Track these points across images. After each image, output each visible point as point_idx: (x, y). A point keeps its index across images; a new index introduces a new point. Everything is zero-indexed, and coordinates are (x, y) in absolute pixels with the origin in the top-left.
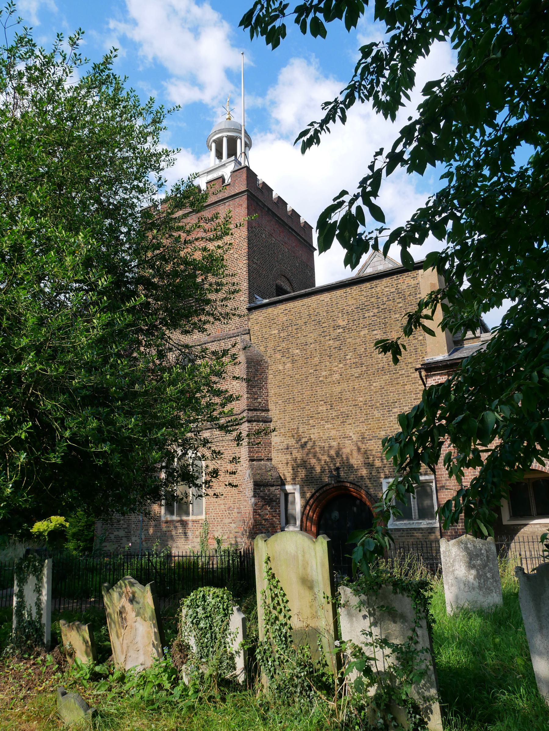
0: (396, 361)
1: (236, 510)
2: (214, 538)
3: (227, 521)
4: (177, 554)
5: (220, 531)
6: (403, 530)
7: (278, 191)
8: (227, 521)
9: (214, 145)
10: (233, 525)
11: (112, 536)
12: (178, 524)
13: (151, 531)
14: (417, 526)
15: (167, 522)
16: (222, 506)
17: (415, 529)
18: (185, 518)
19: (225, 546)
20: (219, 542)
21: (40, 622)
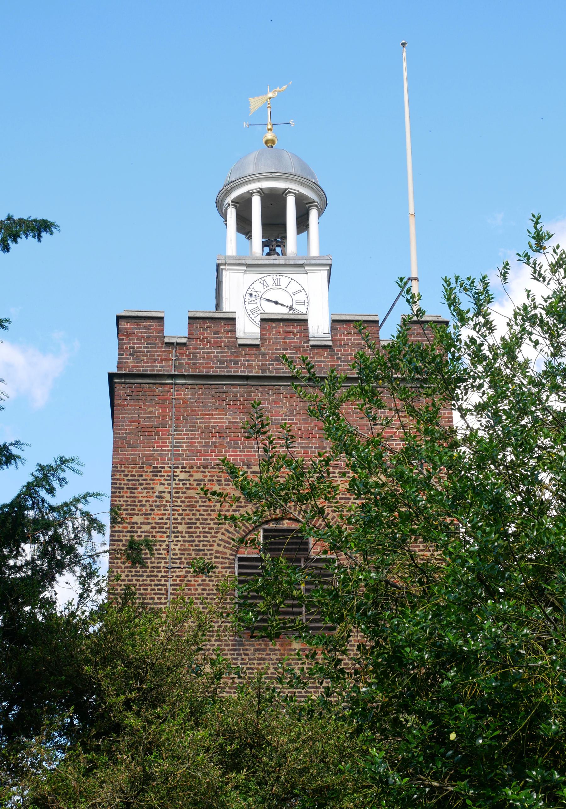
9: (232, 213)
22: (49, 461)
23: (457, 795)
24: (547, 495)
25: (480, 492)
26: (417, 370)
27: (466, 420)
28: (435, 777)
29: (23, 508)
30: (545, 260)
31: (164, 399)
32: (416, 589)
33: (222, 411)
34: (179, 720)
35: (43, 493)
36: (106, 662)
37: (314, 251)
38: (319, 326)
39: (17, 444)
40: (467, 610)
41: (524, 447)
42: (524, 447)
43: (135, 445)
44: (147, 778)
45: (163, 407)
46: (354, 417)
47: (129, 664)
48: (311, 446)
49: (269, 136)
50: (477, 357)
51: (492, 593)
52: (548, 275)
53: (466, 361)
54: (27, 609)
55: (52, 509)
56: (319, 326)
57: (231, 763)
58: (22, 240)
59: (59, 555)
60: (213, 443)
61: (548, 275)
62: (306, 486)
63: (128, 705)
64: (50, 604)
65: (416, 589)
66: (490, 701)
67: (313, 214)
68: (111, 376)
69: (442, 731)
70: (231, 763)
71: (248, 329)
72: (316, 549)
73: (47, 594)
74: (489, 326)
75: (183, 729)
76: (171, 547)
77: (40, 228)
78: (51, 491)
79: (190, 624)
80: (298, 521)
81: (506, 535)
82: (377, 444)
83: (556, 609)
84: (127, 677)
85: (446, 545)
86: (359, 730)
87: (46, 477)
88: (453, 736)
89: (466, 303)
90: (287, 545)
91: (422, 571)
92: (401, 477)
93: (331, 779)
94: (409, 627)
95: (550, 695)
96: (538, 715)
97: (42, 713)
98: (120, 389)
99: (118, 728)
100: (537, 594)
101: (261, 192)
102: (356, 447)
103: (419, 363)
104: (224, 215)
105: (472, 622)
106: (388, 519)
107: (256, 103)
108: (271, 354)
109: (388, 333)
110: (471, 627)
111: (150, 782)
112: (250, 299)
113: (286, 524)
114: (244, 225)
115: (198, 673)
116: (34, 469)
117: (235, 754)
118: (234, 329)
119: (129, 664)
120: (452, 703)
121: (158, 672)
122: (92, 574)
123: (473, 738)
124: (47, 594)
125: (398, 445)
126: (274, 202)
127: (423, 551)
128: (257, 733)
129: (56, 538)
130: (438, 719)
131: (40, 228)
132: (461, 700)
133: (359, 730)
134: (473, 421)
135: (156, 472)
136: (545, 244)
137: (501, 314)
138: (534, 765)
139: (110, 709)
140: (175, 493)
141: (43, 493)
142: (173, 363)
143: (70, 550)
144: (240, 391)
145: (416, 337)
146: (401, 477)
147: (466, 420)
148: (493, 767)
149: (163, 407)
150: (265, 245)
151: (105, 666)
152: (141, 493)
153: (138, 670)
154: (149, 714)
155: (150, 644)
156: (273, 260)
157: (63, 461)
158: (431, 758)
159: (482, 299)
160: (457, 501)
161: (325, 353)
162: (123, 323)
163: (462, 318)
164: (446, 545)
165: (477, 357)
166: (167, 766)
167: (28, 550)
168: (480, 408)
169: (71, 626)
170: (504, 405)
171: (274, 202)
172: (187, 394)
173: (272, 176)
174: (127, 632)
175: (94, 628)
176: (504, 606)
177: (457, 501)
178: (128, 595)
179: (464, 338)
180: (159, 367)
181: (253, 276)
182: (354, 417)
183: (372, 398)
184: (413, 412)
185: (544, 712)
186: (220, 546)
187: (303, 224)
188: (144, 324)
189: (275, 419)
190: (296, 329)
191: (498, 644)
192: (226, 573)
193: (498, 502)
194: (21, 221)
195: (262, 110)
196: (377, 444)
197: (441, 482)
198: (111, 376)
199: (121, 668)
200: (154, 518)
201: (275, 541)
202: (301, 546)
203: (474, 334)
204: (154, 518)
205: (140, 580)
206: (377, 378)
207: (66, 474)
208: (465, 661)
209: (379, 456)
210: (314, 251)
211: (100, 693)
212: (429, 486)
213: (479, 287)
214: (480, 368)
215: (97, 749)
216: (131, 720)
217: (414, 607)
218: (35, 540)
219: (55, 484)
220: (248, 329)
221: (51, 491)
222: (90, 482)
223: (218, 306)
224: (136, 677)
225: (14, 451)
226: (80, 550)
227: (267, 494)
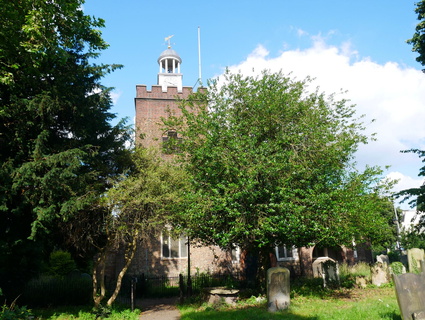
0: (112, 88)
1: (207, 254)
2: (195, 268)
3: (202, 259)
4: (171, 276)
5: (199, 264)
6: (283, 261)
7: (423, 167)
8: (202, 259)
9: (161, 63)
10: (206, 261)
11: (132, 269)
12: (171, 262)
13: (153, 266)
14: (287, 260)
15: (163, 261)
16: (199, 253)
17: (287, 261)
18: (175, 258)
19: (201, 272)
20: (198, 269)
21: (337, 280)
22: (124, 117)
23: (207, 186)
24: (227, 126)
25: (214, 124)
26: (201, 99)
27: (211, 109)
28: (203, 182)
29: (119, 127)
30: (228, 76)
31: (147, 104)
32: (200, 144)
33: (159, 106)
34: (152, 170)
35: (123, 124)
36: (136, 159)
37: (179, 72)
38: (180, 89)
39: (117, 113)
40: (211, 149)
41: (223, 115)
42: (223, 115)
43: (140, 113)
44: (145, 182)
45: (146, 105)
46: (187, 108)
47: (141, 159)
48: (179, 114)
49: (169, 46)
50: (214, 96)
51: (216, 145)
52: (229, 79)
53: (211, 97)
54: (119, 148)
55: (125, 127)
56: (180, 89)
57: (162, 179)
58: (117, 69)
59: (126, 137)
60: (156, 114)
61: (229, 79)
62: (179, 123)
63: (141, 167)
64: (124, 147)
65: (200, 144)
66: (215, 167)
67: (179, 64)
68: (135, 99)
69: (205, 173)
70: (162, 179)
71: (164, 89)
72: (179, 136)
73: (124, 145)
74: (216, 90)
75: (152, 172)
76: (149, 135)
77: (121, 67)
78: (124, 124)
79: (154, 151)
80: (175, 130)
81: (219, 134)
82: (193, 114)
83: (229, 149)
84: (141, 162)
85: (206, 135)
86: (188, 173)
87: (124, 121)
88: (207, 174)
89: (212, 85)
90: (173, 135)
91: (201, 140)
92: (197, 121)
93: (182, 182)
94: (199, 152)
95: (227, 166)
96: (224, 170)
97: (307, 180)
98: (137, 101)
99: (139, 172)
100: (225, 145)
101: (167, 59)
102: (188, 115)
103: (201, 98)
104: (159, 64)
105: (211, 151)
106: (195, 130)
107: (166, 39)
108: (169, 94)
109: (195, 91)
110: (211, 152)
111: (279, 188)
112: (165, 82)
113: (172, 131)
114: (164, 66)
115: (155, 161)
116: (121, 119)
117: (163, 177)
118: (161, 89)
119: (141, 159)
120: (207, 167)
121: (147, 161)
122: (133, 141)
123: (211, 174)
124: (124, 145)
125: (197, 115)
126: (170, 61)
127: (201, 137)
128: (168, 173)
129: (126, 133)
130: (204, 170)
131: (121, 67)
132: (209, 167)
133: (188, 173)
134: (212, 109)
135: (145, 119)
136: (228, 72)
137: (219, 86)
138: (223, 180)
139: (137, 168)
140: (149, 124)
141: (123, 124)
142: (148, 96)
143: (129, 136)
144: (163, 102)
145: (201, 91)
146: (197, 121)
147: (211, 109)
148: (215, 180)
149: (146, 105)
150: (168, 70)
151: (136, 159)
152: (142, 124)
153: (143, 160)
154: (146, 169)
155: (146, 155)
156: (170, 74)
157: (127, 117)
158: (203, 178)
159: (215, 83)
160: (209, 127)
161: (181, 94)
162: (138, 87)
163: (211, 88)
164: (206, 135)
165: (214, 96)
166: (149, 180)
167: (120, 136)
168: (213, 107)
169: (129, 152)
170: (219, 107)
171: (170, 61)
172: (152, 103)
173: (170, 56)
174: (140, 153)
175: (134, 152)
176: (218, 148)
177: (209, 127)
178: (140, 145)
179: (211, 92)
180: (145, 97)
181: (166, 77)
182: (187, 108)
183: (192, 104)
184: (200, 108)
185: (225, 169)
186: (159, 135)
187: (176, 66)
188: (142, 87)
189: (171, 108)
190: (175, 89)
191: (217, 156)
192: (161, 141)
193: (217, 127)
194: (116, 65)
195: (168, 41)
196: (193, 114)
197: (206, 122)
198: (135, 99)
199: (139, 160)
200: (145, 129)
201: (170, 134)
202: (176, 135)
203: (213, 92)
204: (145, 129)
205: (142, 142)
206: (193, 100)
207: (128, 120)
208: (210, 159)
209: (193, 117)
210: (179, 72)
211: (135, 165)
212: (203, 123)
213: (215, 81)
214: (214, 99)
215: (135, 176)
216: (142, 170)
217: (200, 148)
218: (121, 134)
219: (125, 122)
220: (164, 89)
221: (124, 124)
222: (132, 122)
223: (158, 84)
224: (143, 162)
225: (116, 115)
226: (131, 136)
227: (171, 124)
